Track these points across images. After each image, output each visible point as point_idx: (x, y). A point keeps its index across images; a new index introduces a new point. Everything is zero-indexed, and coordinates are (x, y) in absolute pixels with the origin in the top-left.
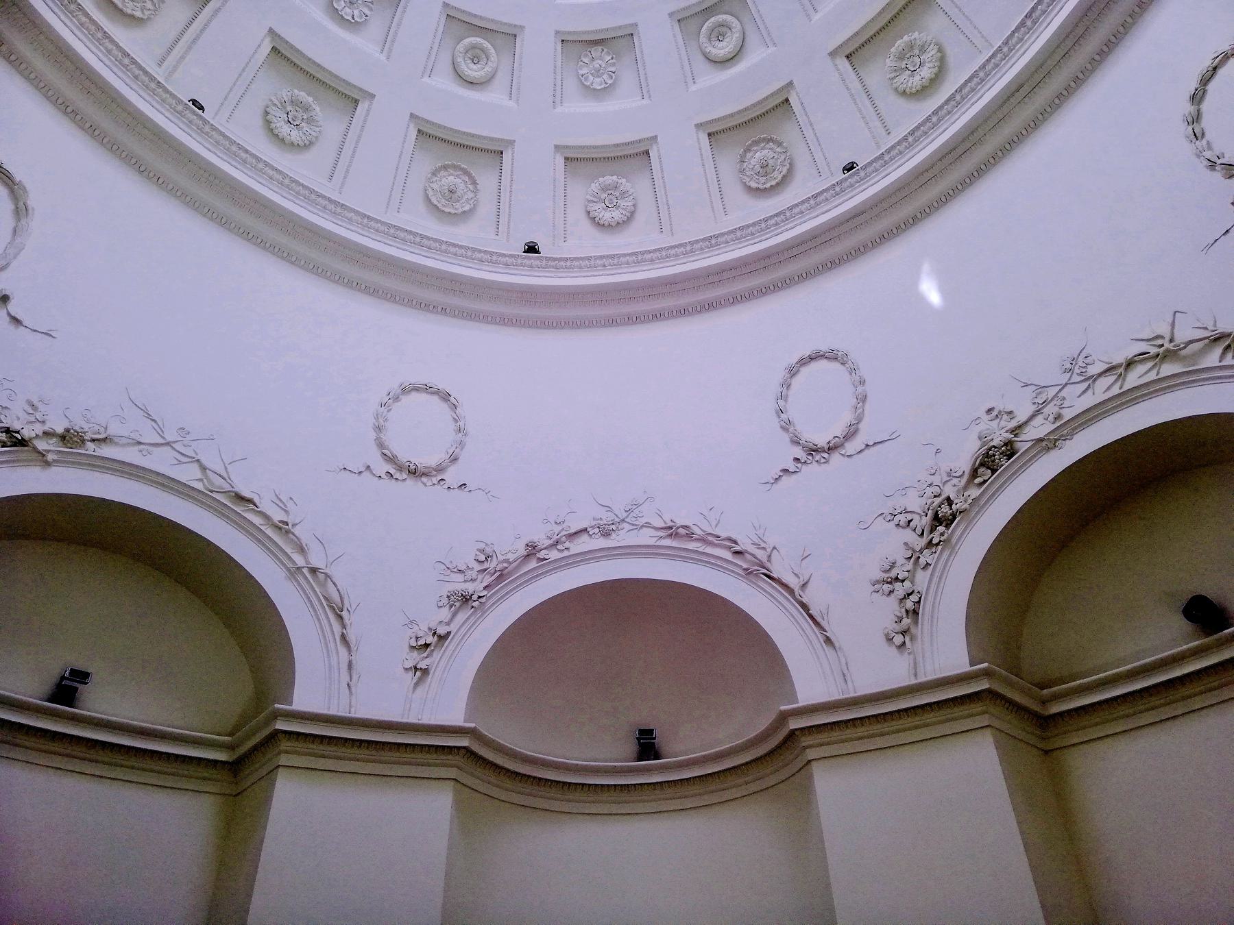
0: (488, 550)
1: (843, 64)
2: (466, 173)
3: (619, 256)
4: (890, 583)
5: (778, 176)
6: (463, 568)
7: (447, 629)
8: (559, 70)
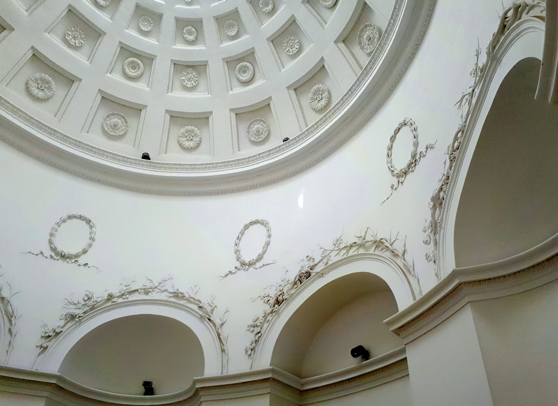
0: (90, 295)
1: (292, 92)
3: (184, 165)
4: (254, 327)
5: (263, 137)
6: (76, 302)
7: (61, 330)
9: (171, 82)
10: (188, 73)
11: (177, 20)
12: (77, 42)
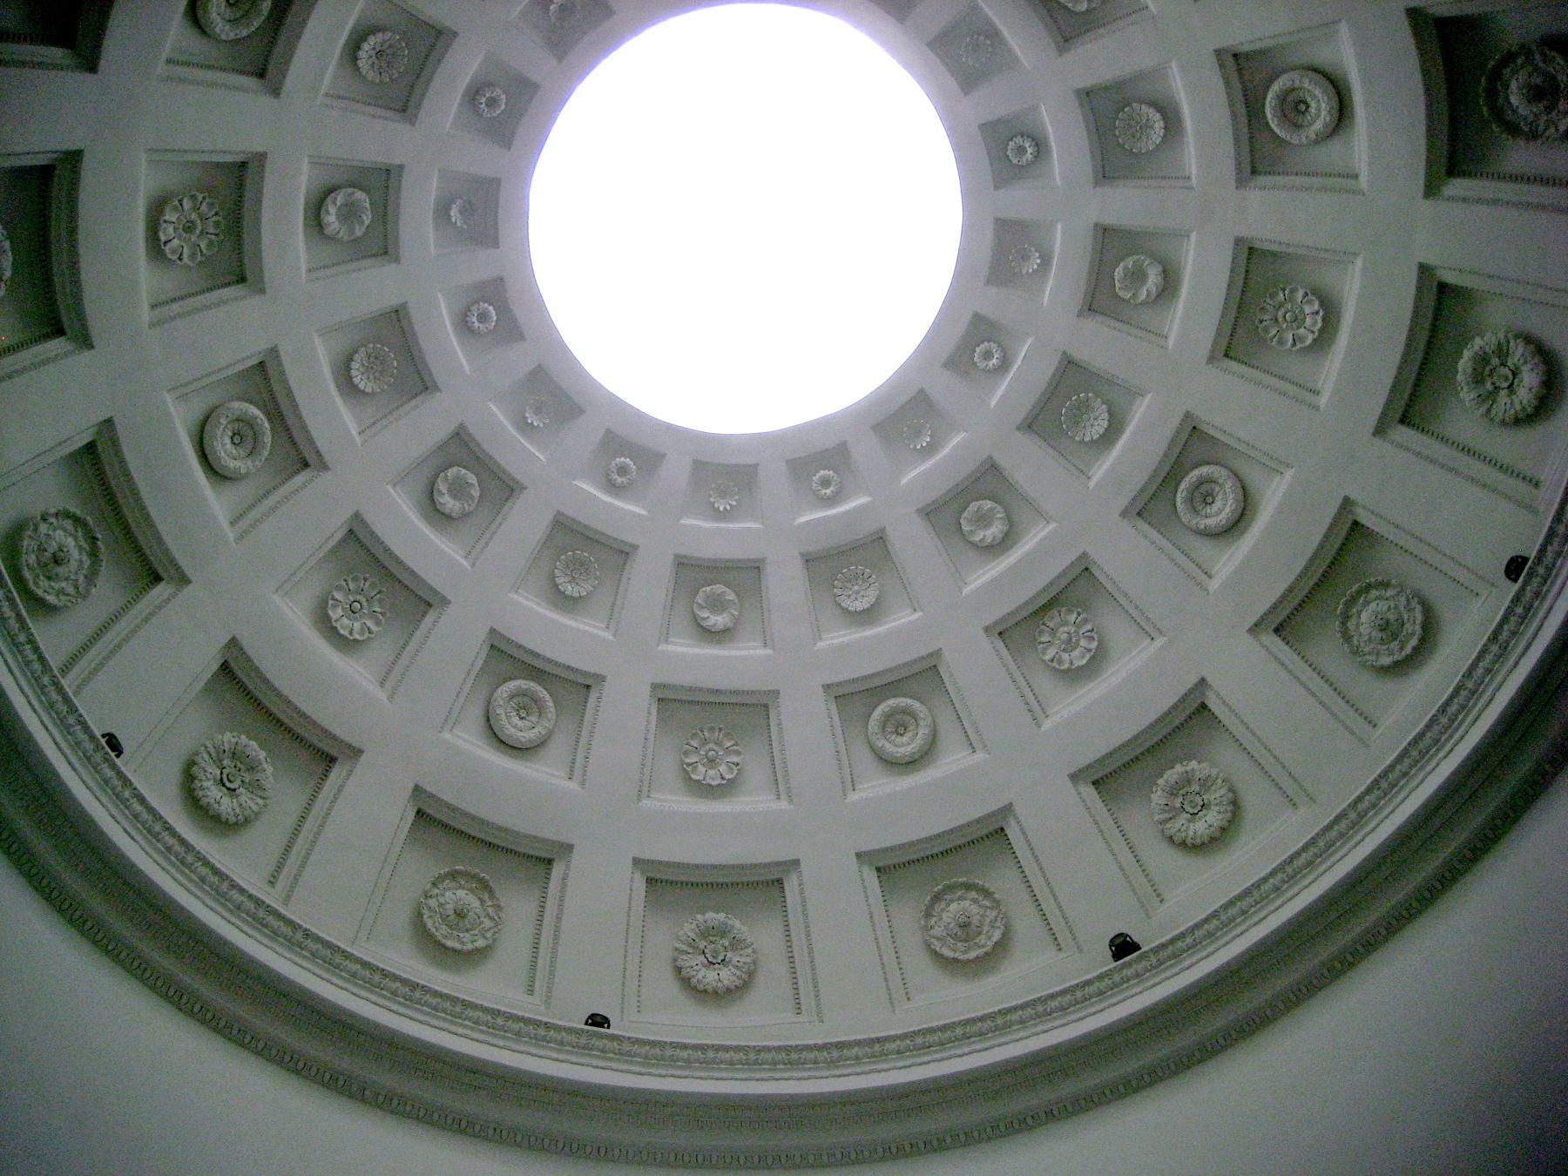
2: (969, 887)
3: (1257, 885)
5: (1414, 627)
8: (1017, 674)
9: (1027, 691)
10: (1053, 631)
12: (723, 768)
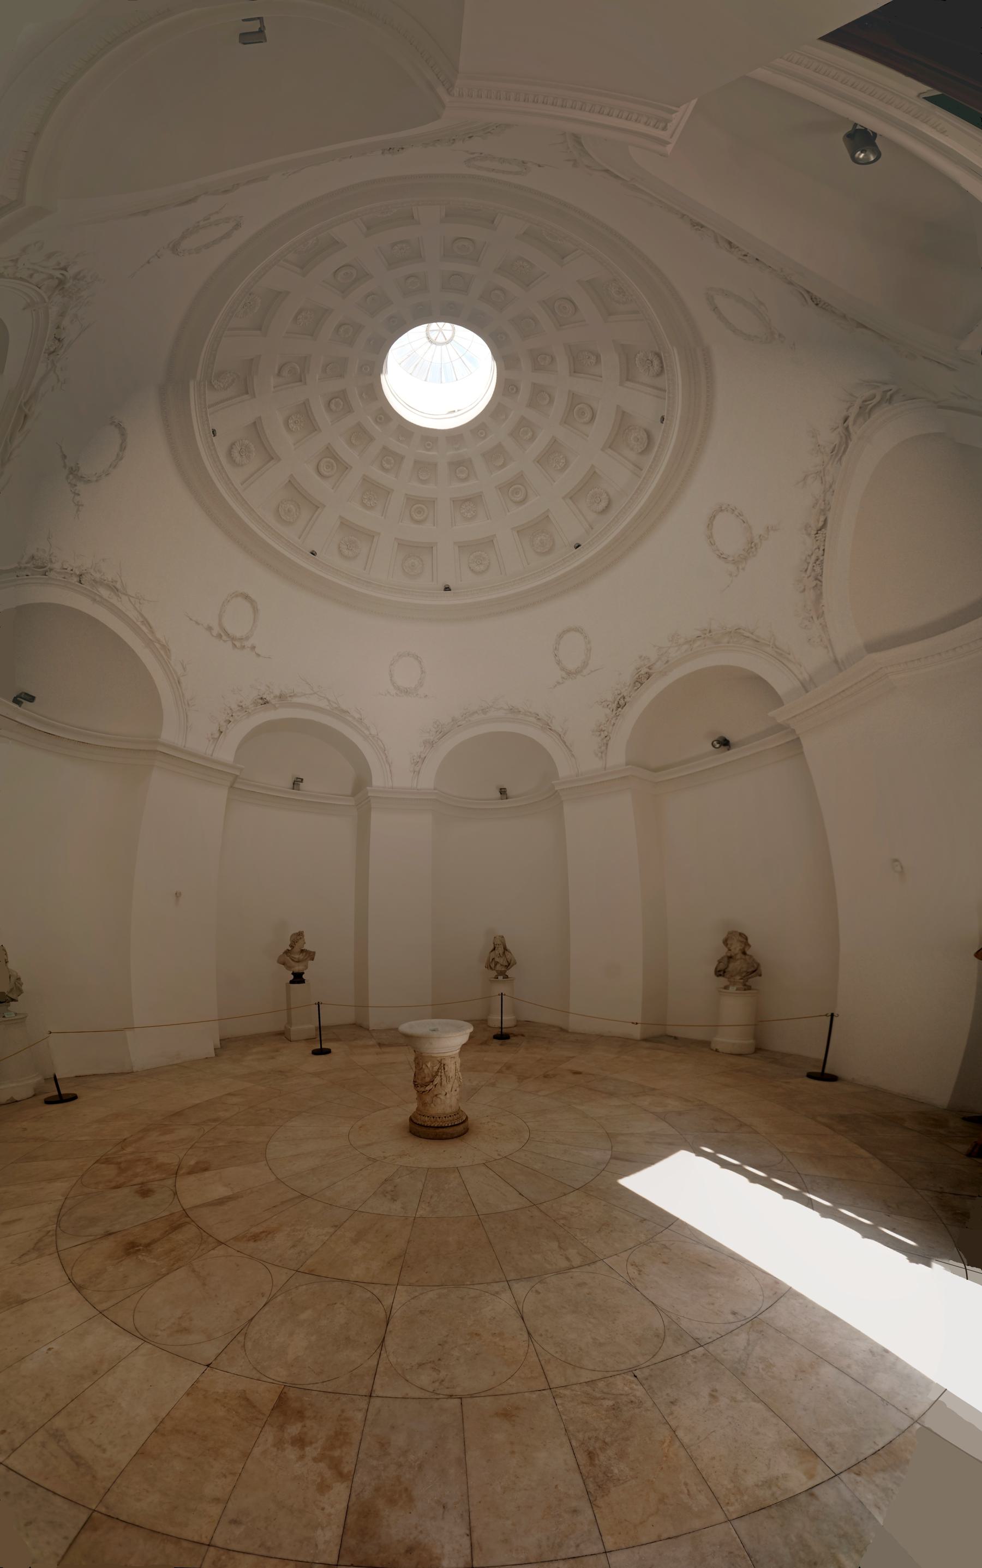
11: (384, 448)
